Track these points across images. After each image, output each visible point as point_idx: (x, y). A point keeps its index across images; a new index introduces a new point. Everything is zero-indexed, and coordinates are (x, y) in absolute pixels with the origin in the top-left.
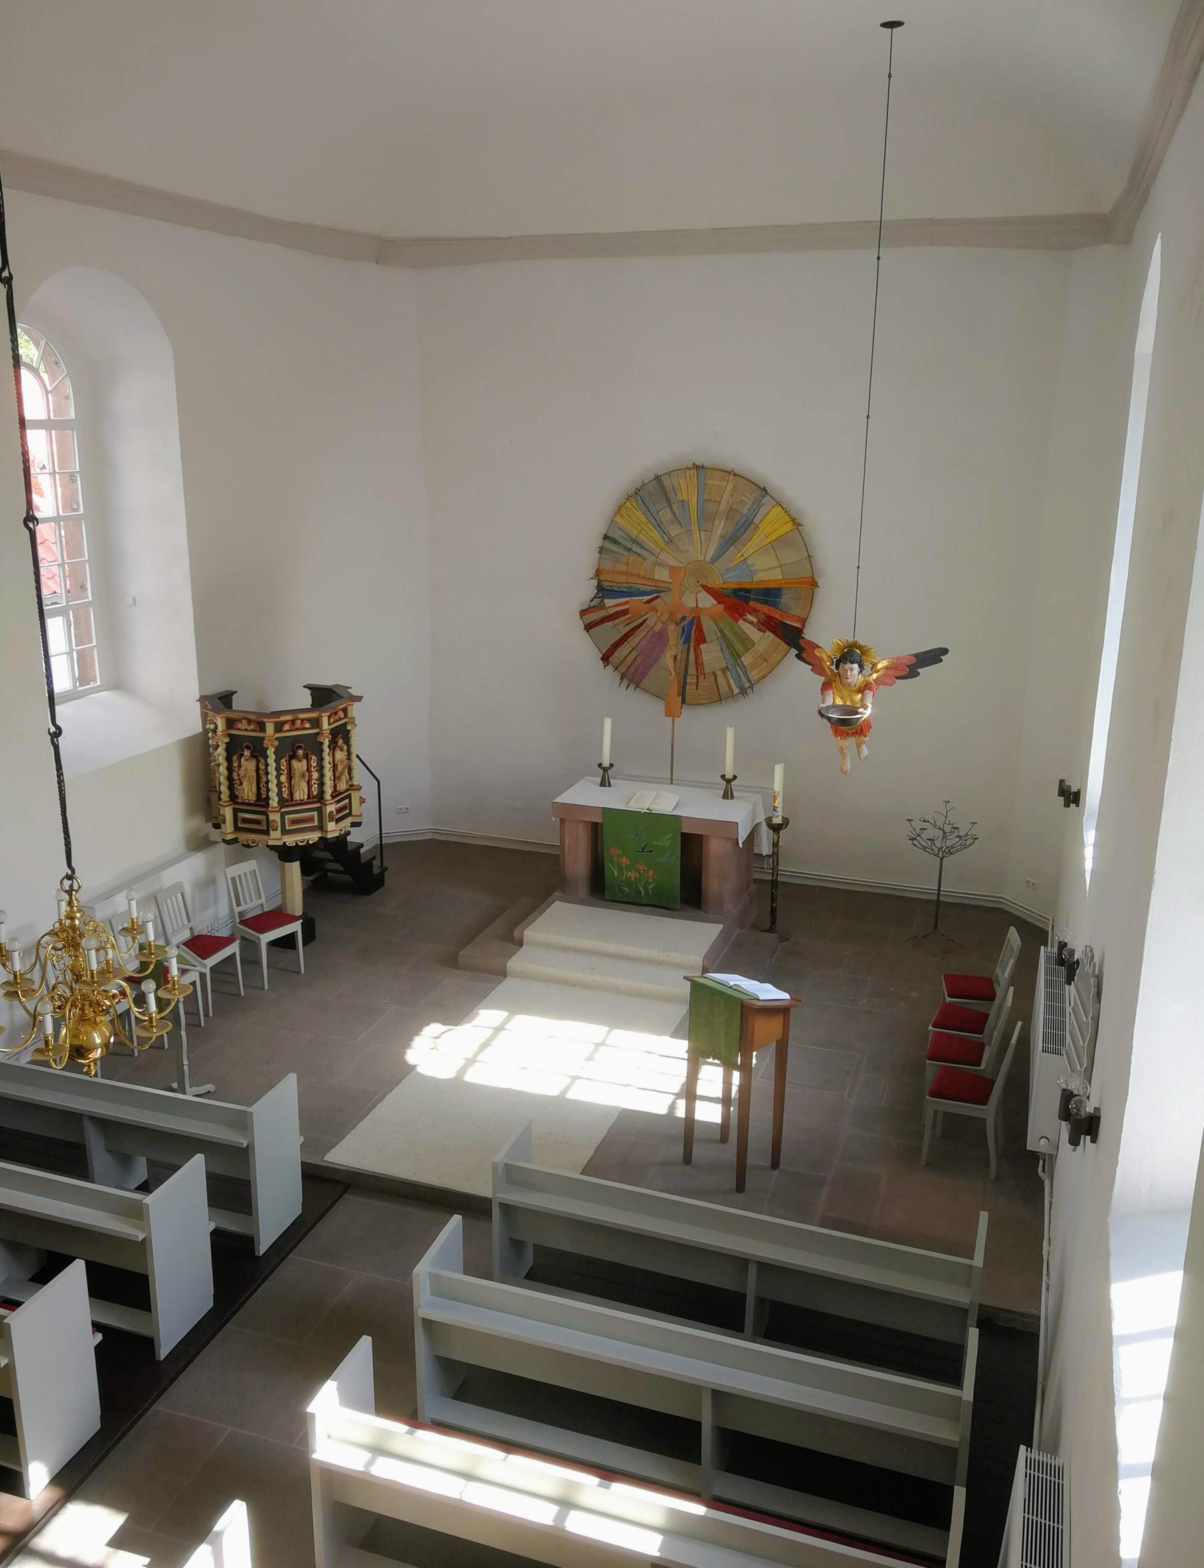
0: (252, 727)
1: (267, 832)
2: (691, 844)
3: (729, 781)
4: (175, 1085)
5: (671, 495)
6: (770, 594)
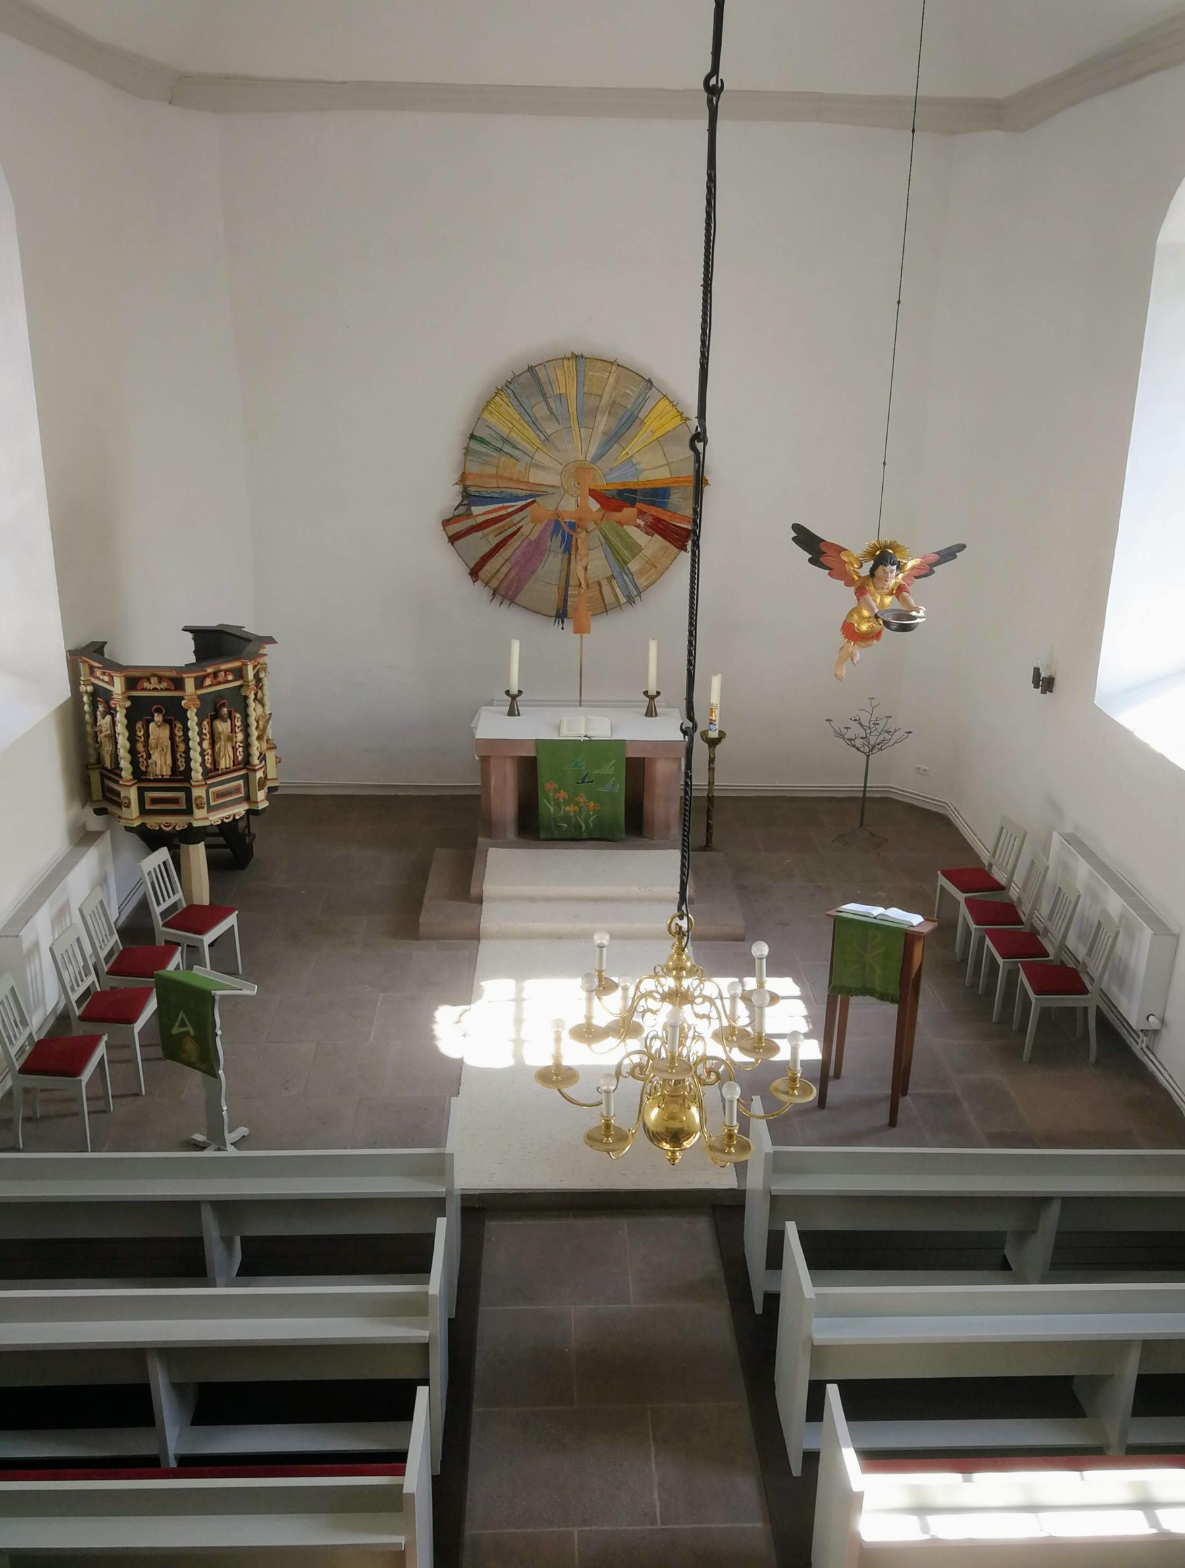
0: (164, 685)
1: (189, 811)
2: (637, 769)
3: (652, 698)
4: (199, 1137)
5: (547, 389)
6: (657, 495)
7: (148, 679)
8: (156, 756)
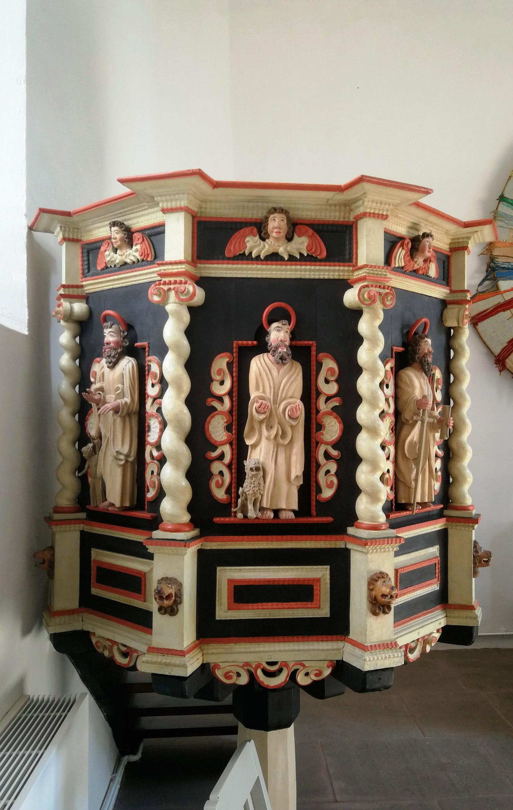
0: (301, 244)
1: (337, 625)
7: (260, 228)
8: (261, 452)
